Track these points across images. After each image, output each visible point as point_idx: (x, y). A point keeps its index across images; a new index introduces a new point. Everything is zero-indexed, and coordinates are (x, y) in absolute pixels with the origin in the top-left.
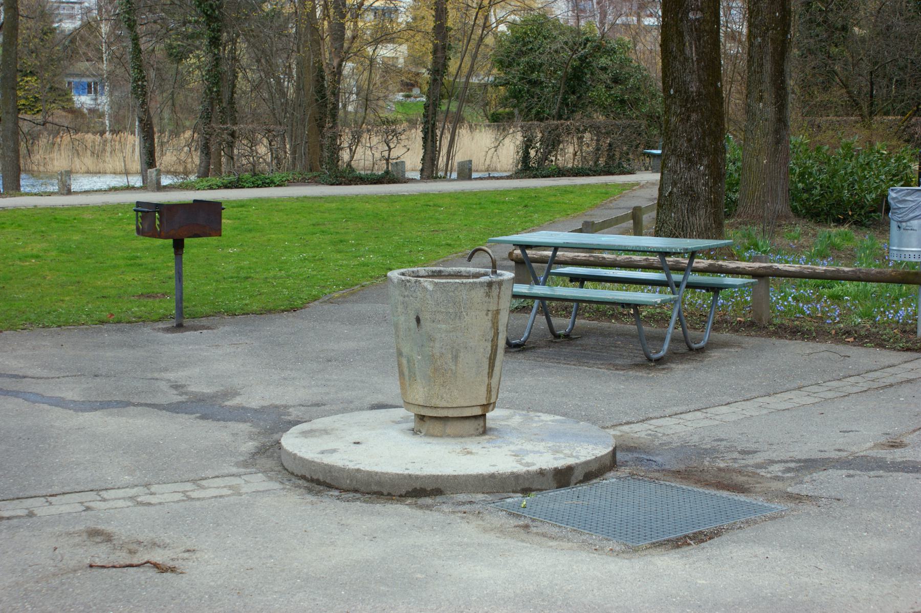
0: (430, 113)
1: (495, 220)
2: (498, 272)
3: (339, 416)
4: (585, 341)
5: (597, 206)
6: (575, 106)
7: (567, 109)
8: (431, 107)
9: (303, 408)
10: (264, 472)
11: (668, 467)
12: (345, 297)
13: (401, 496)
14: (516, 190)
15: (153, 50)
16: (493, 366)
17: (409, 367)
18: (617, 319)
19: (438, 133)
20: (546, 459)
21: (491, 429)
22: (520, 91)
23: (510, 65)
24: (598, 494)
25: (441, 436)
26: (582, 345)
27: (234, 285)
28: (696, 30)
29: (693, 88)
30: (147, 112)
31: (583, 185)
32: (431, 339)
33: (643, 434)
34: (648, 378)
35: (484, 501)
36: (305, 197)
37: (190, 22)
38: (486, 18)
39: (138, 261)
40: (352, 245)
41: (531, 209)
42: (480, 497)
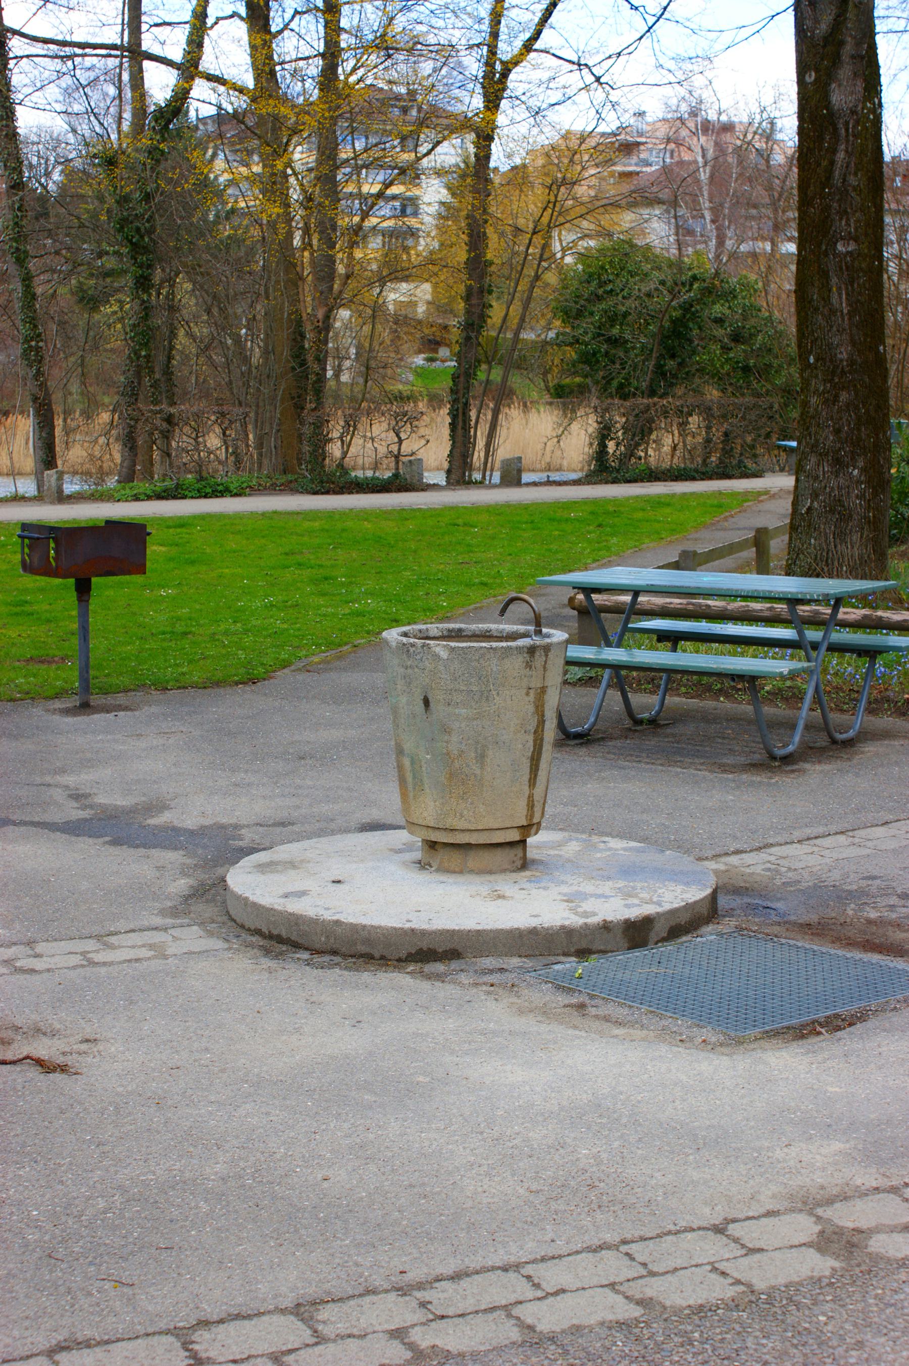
0: (461, 386)
1: (554, 547)
2: (544, 630)
3: (306, 843)
4: (679, 729)
5: (705, 526)
6: (675, 376)
7: (663, 380)
8: (462, 379)
9: (261, 829)
10: (202, 924)
11: (793, 918)
12: (328, 662)
13: (399, 960)
14: (586, 501)
15: (54, 295)
16: (537, 769)
17: (413, 771)
18: (727, 696)
19: (473, 414)
20: (613, 906)
21: (534, 861)
22: (594, 354)
23: (579, 314)
24: (689, 958)
25: (461, 872)
26: (674, 736)
27: (165, 644)
28: (847, 268)
29: (843, 354)
30: (43, 386)
31: (685, 494)
32: (446, 730)
33: (758, 869)
34: (769, 785)
35: (521, 967)
36: (275, 512)
37: (107, 253)
38: (545, 246)
39: (27, 608)
40: (342, 584)
41: (609, 531)
42: (515, 961)
